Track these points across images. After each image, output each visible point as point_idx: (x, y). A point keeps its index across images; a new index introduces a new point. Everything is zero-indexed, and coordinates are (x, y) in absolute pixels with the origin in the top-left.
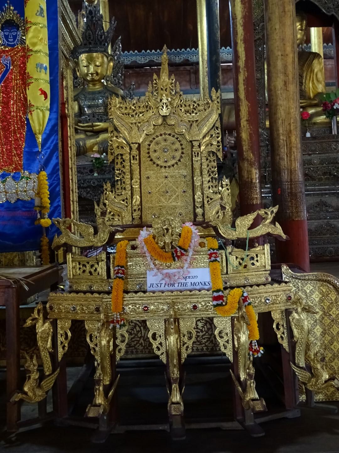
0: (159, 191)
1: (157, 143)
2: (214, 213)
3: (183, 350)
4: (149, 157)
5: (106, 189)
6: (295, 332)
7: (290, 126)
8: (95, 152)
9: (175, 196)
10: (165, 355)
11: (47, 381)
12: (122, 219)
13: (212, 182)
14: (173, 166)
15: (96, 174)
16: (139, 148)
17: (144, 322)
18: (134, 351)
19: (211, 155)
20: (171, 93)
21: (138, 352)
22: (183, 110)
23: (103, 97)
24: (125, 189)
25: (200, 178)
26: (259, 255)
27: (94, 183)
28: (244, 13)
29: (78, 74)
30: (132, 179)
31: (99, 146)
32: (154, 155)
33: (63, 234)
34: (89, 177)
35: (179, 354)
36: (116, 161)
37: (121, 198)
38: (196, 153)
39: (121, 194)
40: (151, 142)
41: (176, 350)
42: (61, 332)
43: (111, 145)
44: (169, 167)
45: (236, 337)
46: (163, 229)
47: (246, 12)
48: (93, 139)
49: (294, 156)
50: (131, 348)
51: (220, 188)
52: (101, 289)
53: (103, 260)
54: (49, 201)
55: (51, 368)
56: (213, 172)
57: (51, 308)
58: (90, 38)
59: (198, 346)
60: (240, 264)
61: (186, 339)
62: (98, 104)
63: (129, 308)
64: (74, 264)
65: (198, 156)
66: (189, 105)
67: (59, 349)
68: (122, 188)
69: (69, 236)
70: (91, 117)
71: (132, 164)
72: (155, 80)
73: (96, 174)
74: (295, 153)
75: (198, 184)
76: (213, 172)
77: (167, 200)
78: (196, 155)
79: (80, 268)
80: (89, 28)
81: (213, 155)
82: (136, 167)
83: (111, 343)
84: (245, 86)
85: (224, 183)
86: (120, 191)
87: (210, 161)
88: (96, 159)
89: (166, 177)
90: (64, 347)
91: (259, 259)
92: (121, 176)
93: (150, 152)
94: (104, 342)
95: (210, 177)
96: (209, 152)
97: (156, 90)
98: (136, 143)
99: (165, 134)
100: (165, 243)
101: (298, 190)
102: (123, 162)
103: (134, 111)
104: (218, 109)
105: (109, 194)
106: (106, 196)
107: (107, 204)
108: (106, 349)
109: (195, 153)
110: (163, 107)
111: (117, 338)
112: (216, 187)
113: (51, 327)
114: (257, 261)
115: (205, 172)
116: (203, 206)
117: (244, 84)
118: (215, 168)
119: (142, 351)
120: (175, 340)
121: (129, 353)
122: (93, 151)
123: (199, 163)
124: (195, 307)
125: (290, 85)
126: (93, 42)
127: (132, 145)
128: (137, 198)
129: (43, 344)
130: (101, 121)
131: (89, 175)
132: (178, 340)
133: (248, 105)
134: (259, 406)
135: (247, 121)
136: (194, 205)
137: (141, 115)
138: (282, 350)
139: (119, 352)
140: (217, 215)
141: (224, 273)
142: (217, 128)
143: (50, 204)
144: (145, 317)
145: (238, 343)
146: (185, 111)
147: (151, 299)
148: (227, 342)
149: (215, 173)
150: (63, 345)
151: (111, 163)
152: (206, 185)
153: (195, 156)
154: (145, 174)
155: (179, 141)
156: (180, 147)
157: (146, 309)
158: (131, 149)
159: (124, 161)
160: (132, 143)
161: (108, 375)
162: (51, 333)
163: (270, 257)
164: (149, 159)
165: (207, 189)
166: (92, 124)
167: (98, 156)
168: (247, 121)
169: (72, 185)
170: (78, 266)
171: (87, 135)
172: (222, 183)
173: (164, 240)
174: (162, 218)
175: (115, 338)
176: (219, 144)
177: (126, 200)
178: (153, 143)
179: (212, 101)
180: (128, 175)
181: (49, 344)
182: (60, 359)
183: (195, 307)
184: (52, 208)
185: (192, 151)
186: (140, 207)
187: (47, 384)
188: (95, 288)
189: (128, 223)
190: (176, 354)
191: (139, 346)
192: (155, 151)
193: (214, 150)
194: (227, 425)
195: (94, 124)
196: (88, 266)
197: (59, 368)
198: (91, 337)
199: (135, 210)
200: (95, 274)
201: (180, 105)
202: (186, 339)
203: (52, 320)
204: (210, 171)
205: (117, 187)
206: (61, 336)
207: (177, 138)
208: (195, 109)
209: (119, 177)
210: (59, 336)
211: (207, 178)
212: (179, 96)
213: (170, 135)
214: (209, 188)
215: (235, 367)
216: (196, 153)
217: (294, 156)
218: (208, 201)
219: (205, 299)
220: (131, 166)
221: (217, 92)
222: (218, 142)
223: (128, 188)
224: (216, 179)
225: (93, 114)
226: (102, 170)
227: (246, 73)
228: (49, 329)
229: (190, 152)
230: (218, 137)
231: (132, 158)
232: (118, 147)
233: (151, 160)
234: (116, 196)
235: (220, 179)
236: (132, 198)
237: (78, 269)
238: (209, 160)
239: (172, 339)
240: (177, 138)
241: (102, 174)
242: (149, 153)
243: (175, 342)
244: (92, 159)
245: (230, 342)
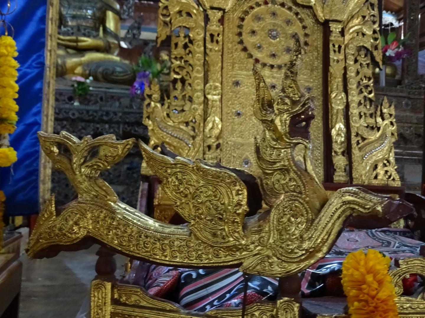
1: (258, 18)
2: (368, 168)
4: (241, 42)
8: (78, 74)
13: (365, 106)
15: (76, 104)
19: (363, 53)
23: (93, 7)
24: (191, 99)
25: (343, 95)
27: (73, 114)
30: (206, 81)
31: (83, 68)
32: (249, 40)
33: (83, 197)
34: (67, 106)
36: (174, 40)
39: (183, 111)
40: (246, 13)
43: (166, 8)
46: (305, 194)
48: (77, 57)
51: (379, 120)
54: (16, 107)
62: (86, 15)
65: (339, 51)
68: (184, 96)
69: (113, 211)
70: (75, 30)
71: (208, 51)
73: (76, 104)
75: (338, 106)
76: (367, 86)
78: (337, 49)
81: (366, 56)
82: (214, 57)
85: (385, 111)
88: (79, 83)
92: (184, 73)
93: (244, 34)
95: (362, 96)
98: (219, 9)
102: (190, 45)
105: (156, 106)
106: (150, 110)
107: (150, 128)
109: (334, 46)
112: (371, 115)
115: (353, 86)
116: (348, 152)
118: (370, 79)
122: (74, 74)
123: (342, 65)
127: (209, 12)
128: (214, 121)
130: (89, 36)
131: (67, 103)
140: (375, 172)
143: (17, 113)
149: (369, 89)
151: (163, 42)
152: (354, 111)
153: (335, 51)
155: (301, 20)
158: (207, 19)
160: (212, 8)
164: (240, 47)
165: (356, 118)
166: (77, 38)
167: (82, 80)
171: (68, 52)
172: (381, 111)
178: (250, 16)
180: (198, 72)
184: (22, 127)
192: (253, 32)
193: (368, 45)
199: (209, 147)
204: (361, 83)
205: (173, 94)
209: (178, 73)
211: (355, 98)
214: (361, 117)
216: (337, 46)
218: (358, 143)
220: (205, 53)
222: (375, 32)
223: (198, 97)
224: (371, 100)
226: (85, 99)
231: (208, 38)
232: (180, 12)
233: (245, 49)
236: (205, 120)
240: (297, 14)
241: (86, 105)
242: (240, 34)
244: (72, 83)
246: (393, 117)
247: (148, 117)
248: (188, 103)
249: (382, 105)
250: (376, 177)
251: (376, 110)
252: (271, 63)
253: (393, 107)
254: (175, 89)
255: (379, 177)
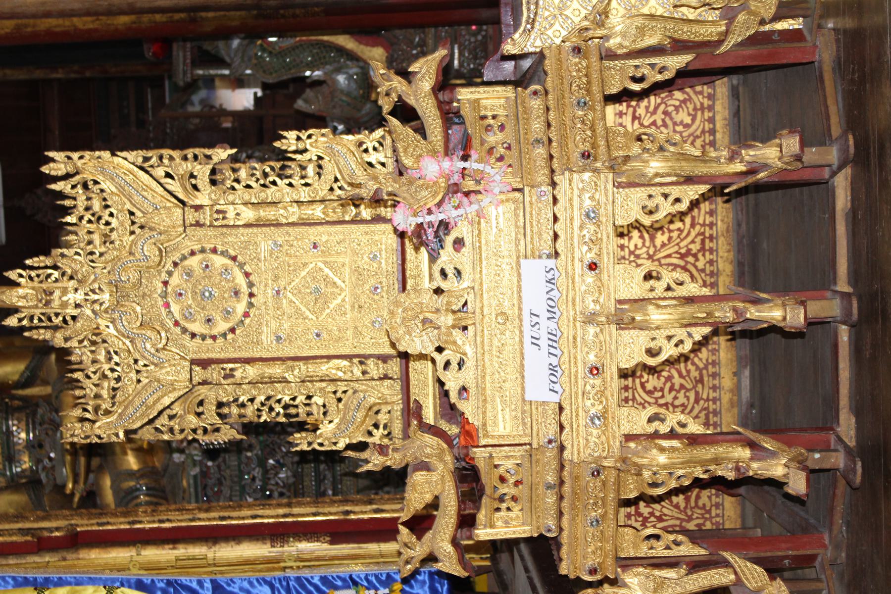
0: (314, 313)
3: (682, 291)
4: (224, 335)
5: (310, 444)
6: (651, 41)
9: (327, 271)
10: (692, 330)
11: (747, 579)
12: (387, 403)
14: (247, 275)
16: (205, 364)
17: (624, 374)
18: (711, 369)
20: (57, 280)
21: (714, 361)
22: (103, 249)
26: (483, 113)
35: (690, 300)
37: (332, 408)
38: (216, 216)
39: (324, 406)
40: (184, 330)
41: (681, 310)
42: (645, 548)
44: (251, 285)
45: (658, 180)
50: (706, 379)
51: (307, 156)
52: (554, 465)
53: (491, 457)
55: (721, 570)
56: (266, 175)
57: (593, 572)
59: (703, 212)
60: (501, 159)
61: (660, 286)
63: (593, 405)
64: (499, 523)
66: (90, 232)
67: (682, 554)
68: (306, 405)
72: (20, 320)
77: (337, 291)
78: (221, 216)
79: (508, 509)
83: (665, 443)
85: (293, 148)
86: (314, 409)
87: (237, 181)
89: (278, 292)
90: (677, 544)
91: (489, 114)
94: (662, 459)
97: (50, 319)
99: (164, 295)
100: (454, 327)
103: (105, 376)
104: (99, 157)
106: (326, 443)
107: (348, 441)
108: (676, 454)
109: (217, 220)
110: (95, 302)
111: (656, 432)
112: (303, 168)
113: (635, 570)
114: (494, 117)
119: (714, 352)
120: (660, 311)
121: (716, 382)
124: (593, 266)
129: (669, 586)
132: (662, 303)
134: (792, 144)
136: (353, 222)
137: (116, 359)
138: (688, 68)
139: (684, 426)
141: (521, 198)
142: (146, 159)
144: (611, 373)
145: (669, 175)
146: (105, 243)
147: (575, 358)
148: (666, 196)
149: (268, 170)
150: (673, 546)
152: (304, 194)
153: (224, 218)
154: (268, 347)
156: (198, 257)
157: (595, 370)
159: (236, 400)
160: (191, 380)
161: (731, 449)
162: (647, 571)
163: (513, 536)
170: (503, 513)
173: (448, 328)
174: (401, 332)
175: (656, 435)
176: (190, 156)
177: (339, 395)
179: (77, 173)
181: (670, 573)
182: (703, 552)
183: (593, 266)
185: (211, 225)
186: (356, 360)
187: (753, 578)
188: (551, 478)
189: (398, 388)
190: (688, 309)
191: (701, 359)
194: (842, 199)
196: (503, 489)
197: (721, 553)
198: (654, 485)
199: (364, 373)
200: (522, 475)
201: (90, 257)
202: (660, 286)
203: (619, 570)
204: (262, 182)
206: (652, 548)
207: (175, 264)
208: (100, 218)
210: (652, 553)
212: (65, 261)
213: (166, 283)
215: (719, 181)
216: (216, 216)
219: (576, 244)
221: (53, 160)
228: (639, 574)
229: (211, 232)
230: (171, 158)
234: (329, 418)
235: (282, 156)
237: (510, 513)
239: (656, 316)
243: (664, 311)
245: (666, 190)
246: (301, 135)
247: (335, 444)
248: (314, 400)
249: (286, 151)
250: (383, 165)
251: (294, 160)
252: (247, 297)
253: (285, 134)
254: (297, 415)
255: (383, 160)
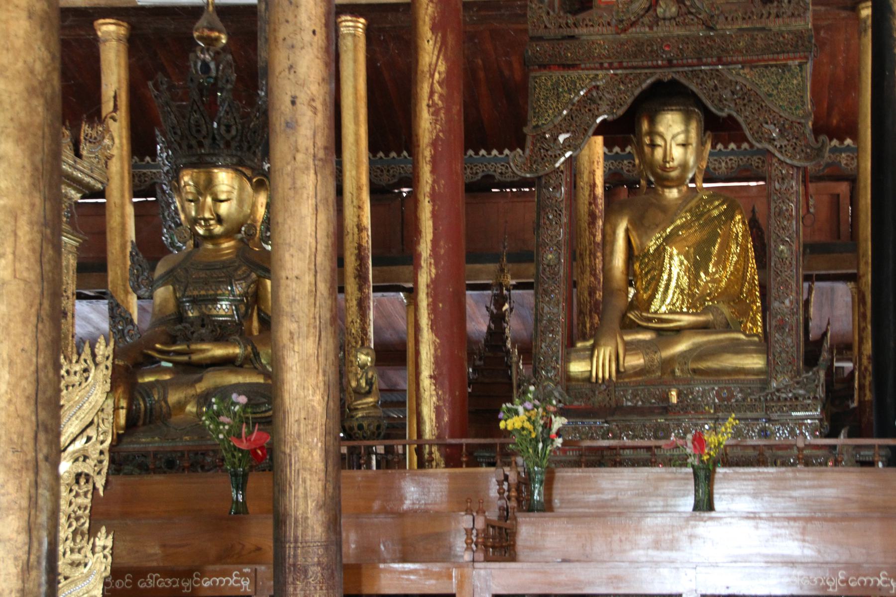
7: (299, 425)
28: (434, 134)
29: (182, 217)
47: (440, 131)
49: (305, 488)
56: (77, 519)
58: (198, 131)
74: (308, 483)
80: (195, 107)
81: (87, 482)
84: (431, 300)
87: (77, 495)
96: (78, 476)
101: (310, 560)
117: (427, 294)
125: (301, 340)
126: (207, 142)
133: (434, 342)
135: (431, 377)
166: (188, 346)
168: (431, 377)
169: (291, 472)
195: (193, 347)
217: (305, 488)
225: (203, 320)
227: (434, 271)
235: (92, 532)
238: (74, 493)
